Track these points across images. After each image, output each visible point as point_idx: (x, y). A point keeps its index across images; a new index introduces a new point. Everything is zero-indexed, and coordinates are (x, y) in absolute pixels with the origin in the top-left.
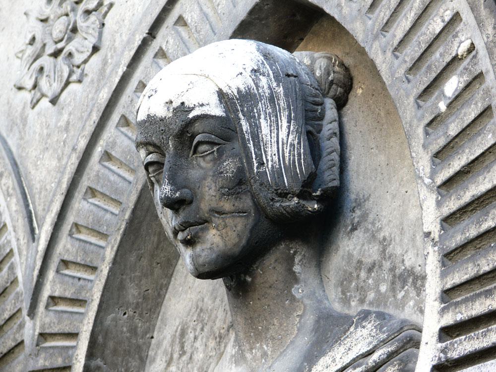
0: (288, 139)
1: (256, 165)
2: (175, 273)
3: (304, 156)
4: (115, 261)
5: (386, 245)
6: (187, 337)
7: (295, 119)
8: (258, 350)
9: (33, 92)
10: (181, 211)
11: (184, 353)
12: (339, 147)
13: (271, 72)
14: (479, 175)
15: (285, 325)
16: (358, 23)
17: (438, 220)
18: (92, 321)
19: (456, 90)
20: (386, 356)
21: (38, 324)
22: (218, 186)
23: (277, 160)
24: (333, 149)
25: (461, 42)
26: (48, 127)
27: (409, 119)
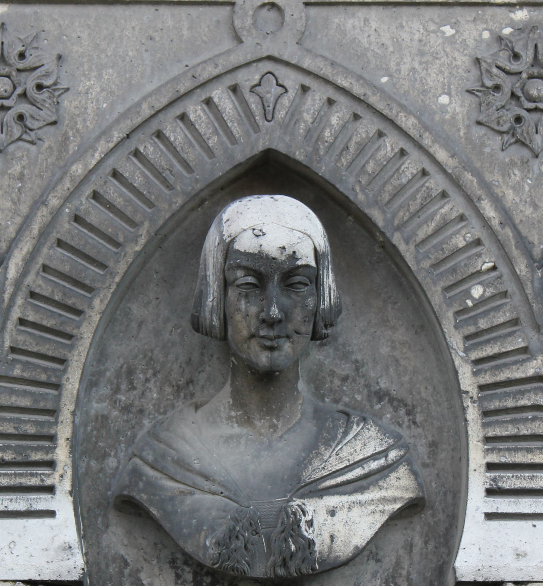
25: (485, 262)
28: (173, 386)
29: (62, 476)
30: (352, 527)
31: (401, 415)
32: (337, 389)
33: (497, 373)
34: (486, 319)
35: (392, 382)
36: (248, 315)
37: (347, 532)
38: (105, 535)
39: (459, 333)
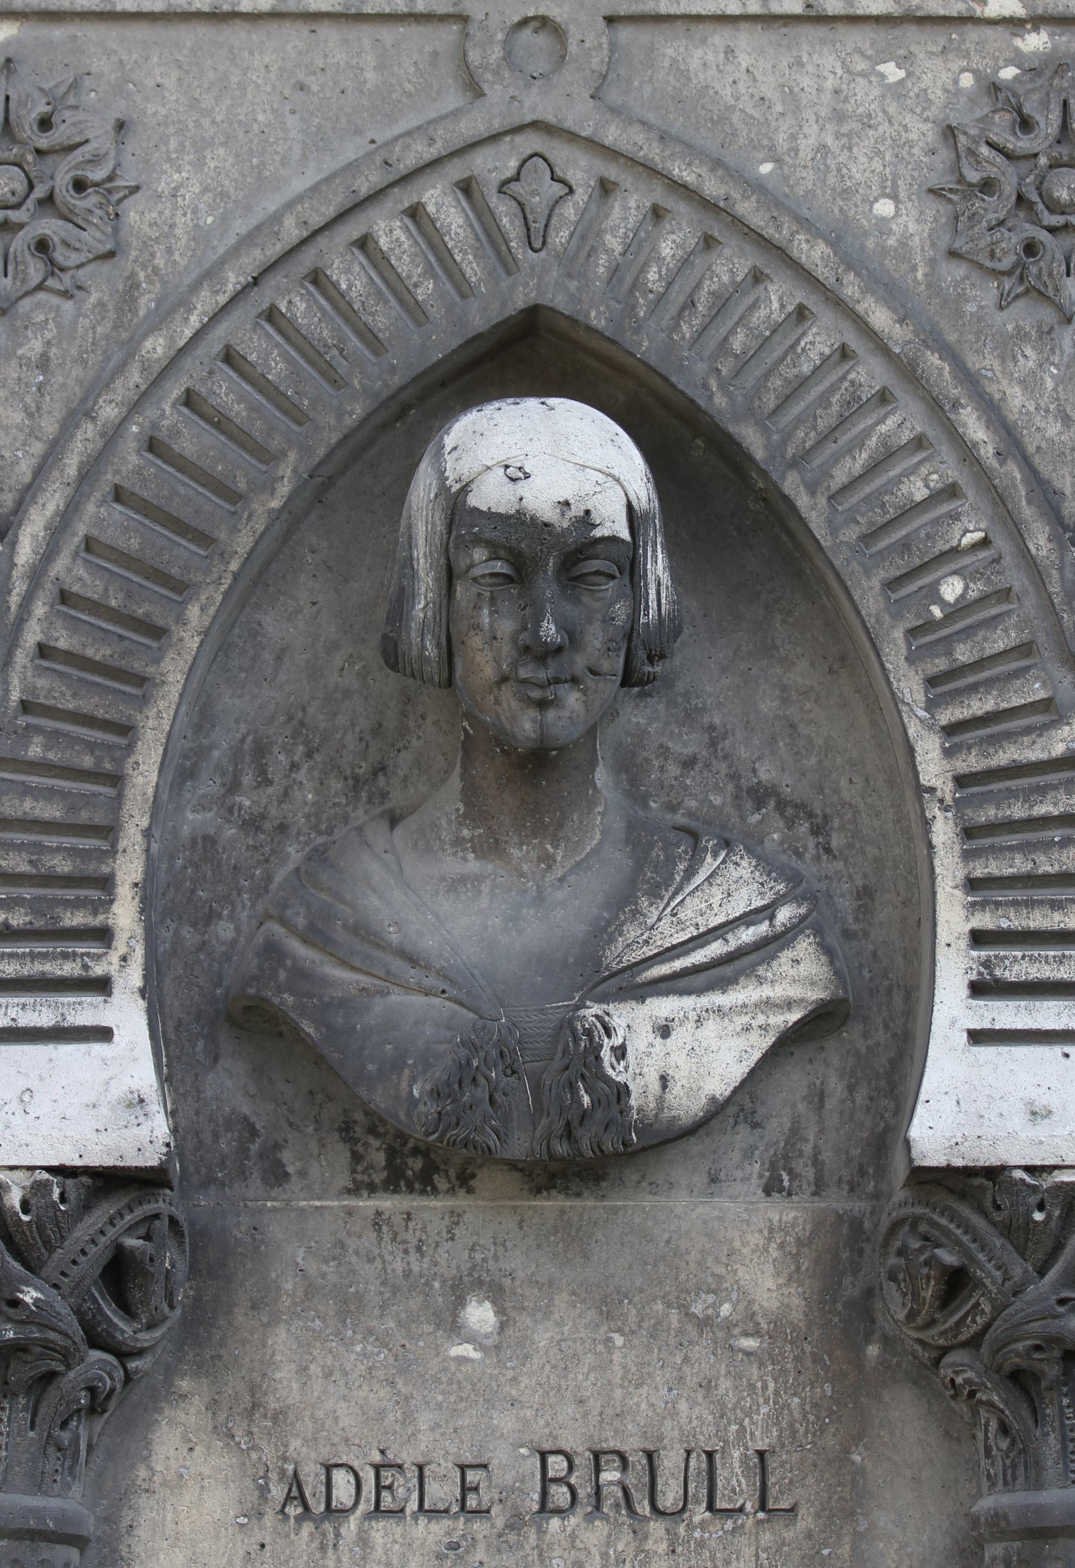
25: (967, 531)
28: (346, 779)
29: (124, 959)
30: (705, 1060)
34: (970, 643)
35: (783, 769)
36: (495, 638)
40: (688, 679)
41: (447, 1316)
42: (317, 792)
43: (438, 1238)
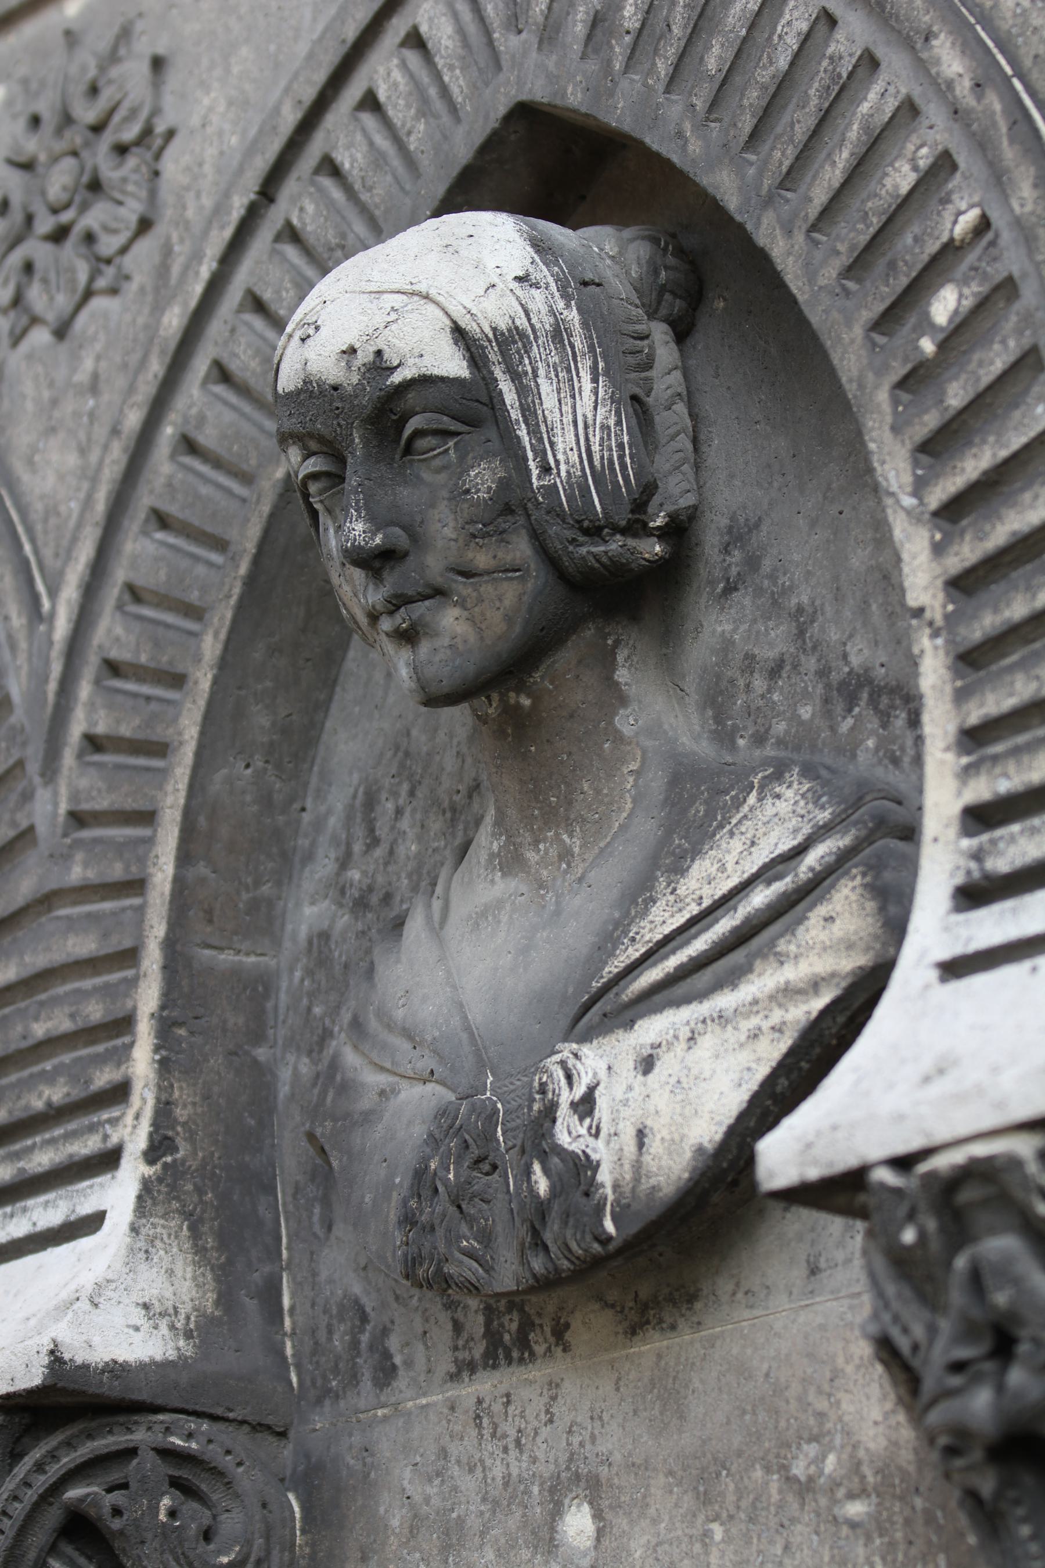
0: (595, 416)
1: (535, 472)
2: (341, 678)
3: (630, 448)
4: (223, 664)
5: (805, 623)
6: (379, 809)
7: (607, 373)
8: (551, 844)
9: (12, 314)
10: (385, 574)
11: (374, 841)
12: (689, 423)
13: (550, 280)
14: (1022, 490)
15: (605, 791)
16: (725, 173)
17: (939, 583)
18: (183, 786)
19: (956, 312)
20: (833, 858)
21: (63, 791)
22: (460, 521)
23: (577, 460)
24: (678, 427)
25: (960, 213)
26: (51, 384)
27: (855, 373)
28: (444, 812)
30: (692, 1094)
31: (898, 732)
32: (761, 703)
33: (988, 527)
34: (964, 377)
35: (876, 643)
37: (678, 1110)
38: (326, 1251)
39: (903, 442)
40: (775, 551)
41: (545, 1533)
42: (419, 839)
43: (536, 1423)
